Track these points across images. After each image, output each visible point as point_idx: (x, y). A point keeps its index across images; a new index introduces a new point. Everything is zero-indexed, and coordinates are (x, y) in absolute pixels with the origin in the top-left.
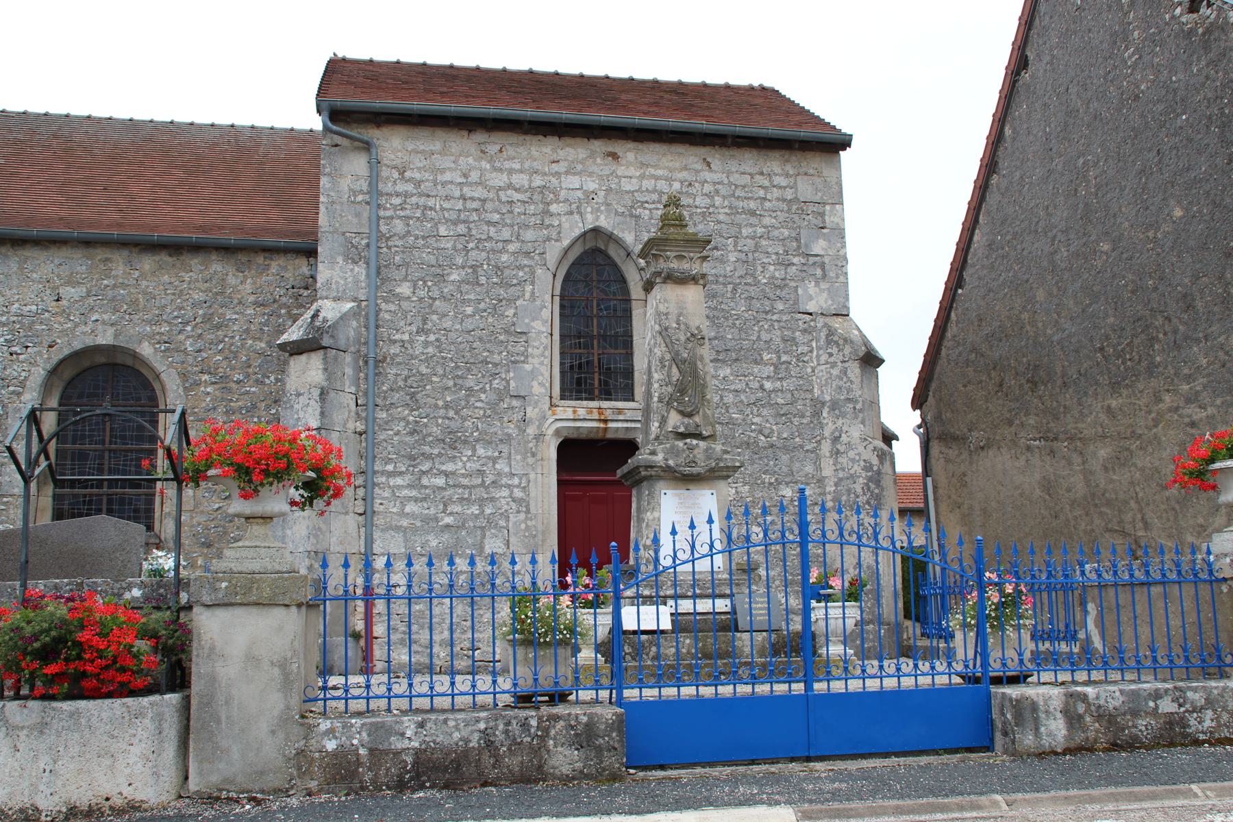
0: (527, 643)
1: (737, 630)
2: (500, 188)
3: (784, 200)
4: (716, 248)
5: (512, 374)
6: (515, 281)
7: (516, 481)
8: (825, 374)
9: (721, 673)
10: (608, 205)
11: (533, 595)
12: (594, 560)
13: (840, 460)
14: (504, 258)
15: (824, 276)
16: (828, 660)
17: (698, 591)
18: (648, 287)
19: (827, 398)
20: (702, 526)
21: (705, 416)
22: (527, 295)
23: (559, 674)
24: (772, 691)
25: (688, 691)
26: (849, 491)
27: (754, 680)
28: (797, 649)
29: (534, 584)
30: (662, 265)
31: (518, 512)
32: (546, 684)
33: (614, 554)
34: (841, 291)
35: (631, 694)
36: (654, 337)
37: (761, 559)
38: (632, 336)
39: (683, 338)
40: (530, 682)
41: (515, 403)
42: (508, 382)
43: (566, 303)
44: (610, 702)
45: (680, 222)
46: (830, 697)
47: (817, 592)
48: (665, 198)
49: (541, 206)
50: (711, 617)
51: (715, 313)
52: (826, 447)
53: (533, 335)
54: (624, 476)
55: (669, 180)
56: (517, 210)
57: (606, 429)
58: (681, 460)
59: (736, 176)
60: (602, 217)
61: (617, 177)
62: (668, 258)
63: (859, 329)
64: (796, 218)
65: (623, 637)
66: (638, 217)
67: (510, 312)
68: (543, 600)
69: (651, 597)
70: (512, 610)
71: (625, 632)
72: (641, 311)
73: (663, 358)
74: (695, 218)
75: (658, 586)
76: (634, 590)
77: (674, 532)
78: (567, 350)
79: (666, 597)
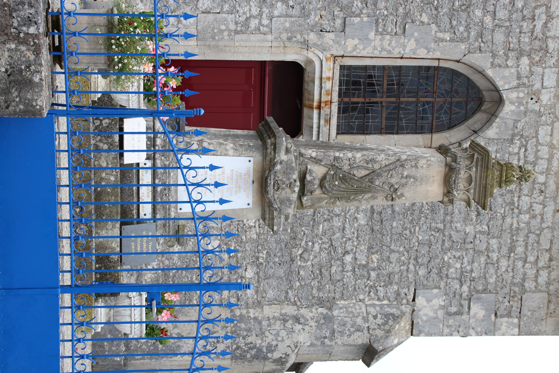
0: (110, 27)
1: (122, 224)
2: (548, 8)
3: (524, 280)
4: (479, 214)
5: (365, 19)
6: (454, 23)
7: (265, 22)
8: (358, 311)
9: (82, 209)
10: (525, 113)
11: (156, 35)
12: (188, 93)
13: (278, 323)
14: (478, 13)
15: (449, 314)
16: (92, 307)
17: (159, 189)
18: (443, 150)
19: (335, 313)
20: (218, 193)
21: (320, 200)
22: (440, 35)
23: (80, 57)
24: (63, 255)
25: (64, 177)
26: (249, 330)
27: (75, 239)
28: (103, 279)
29: (166, 36)
30: (463, 163)
31: (236, 23)
32: (70, 43)
33: (193, 113)
34: (434, 330)
35: (62, 124)
36: (395, 154)
37: (189, 248)
38: (397, 133)
39: (393, 181)
40: (73, 29)
41: (339, 22)
42: (358, 15)
43: (431, 72)
44: (53, 104)
45: (504, 181)
46: (56, 309)
47: (155, 297)
48: (529, 167)
49: (528, 48)
50: (135, 200)
51: (417, 212)
52: (290, 310)
53: (402, 41)
54: (267, 123)
55: (547, 172)
56: (525, 24)
57: (311, 107)
58: (280, 176)
59: (549, 236)
60: (513, 108)
61: (553, 122)
62: (470, 169)
63: (399, 344)
64: (506, 290)
65: (117, 118)
66: (511, 141)
67: (425, 18)
68: (151, 46)
69: (154, 146)
70: (141, 14)
71: (121, 120)
72: (421, 143)
73: (375, 162)
74: (509, 196)
75: (164, 151)
76: (161, 130)
77: (212, 168)
78: (386, 72)
79: (154, 159)
